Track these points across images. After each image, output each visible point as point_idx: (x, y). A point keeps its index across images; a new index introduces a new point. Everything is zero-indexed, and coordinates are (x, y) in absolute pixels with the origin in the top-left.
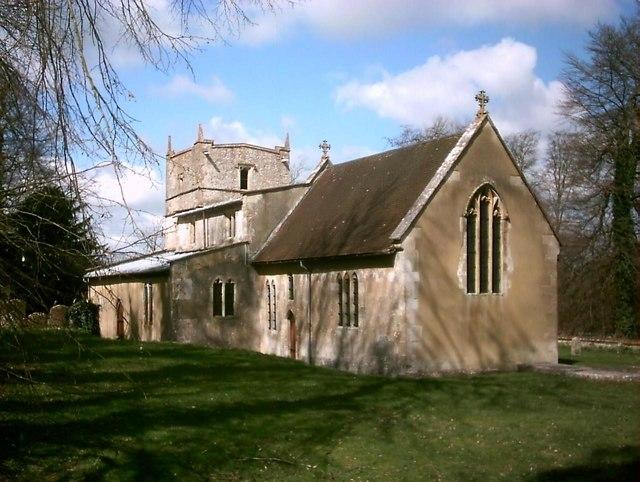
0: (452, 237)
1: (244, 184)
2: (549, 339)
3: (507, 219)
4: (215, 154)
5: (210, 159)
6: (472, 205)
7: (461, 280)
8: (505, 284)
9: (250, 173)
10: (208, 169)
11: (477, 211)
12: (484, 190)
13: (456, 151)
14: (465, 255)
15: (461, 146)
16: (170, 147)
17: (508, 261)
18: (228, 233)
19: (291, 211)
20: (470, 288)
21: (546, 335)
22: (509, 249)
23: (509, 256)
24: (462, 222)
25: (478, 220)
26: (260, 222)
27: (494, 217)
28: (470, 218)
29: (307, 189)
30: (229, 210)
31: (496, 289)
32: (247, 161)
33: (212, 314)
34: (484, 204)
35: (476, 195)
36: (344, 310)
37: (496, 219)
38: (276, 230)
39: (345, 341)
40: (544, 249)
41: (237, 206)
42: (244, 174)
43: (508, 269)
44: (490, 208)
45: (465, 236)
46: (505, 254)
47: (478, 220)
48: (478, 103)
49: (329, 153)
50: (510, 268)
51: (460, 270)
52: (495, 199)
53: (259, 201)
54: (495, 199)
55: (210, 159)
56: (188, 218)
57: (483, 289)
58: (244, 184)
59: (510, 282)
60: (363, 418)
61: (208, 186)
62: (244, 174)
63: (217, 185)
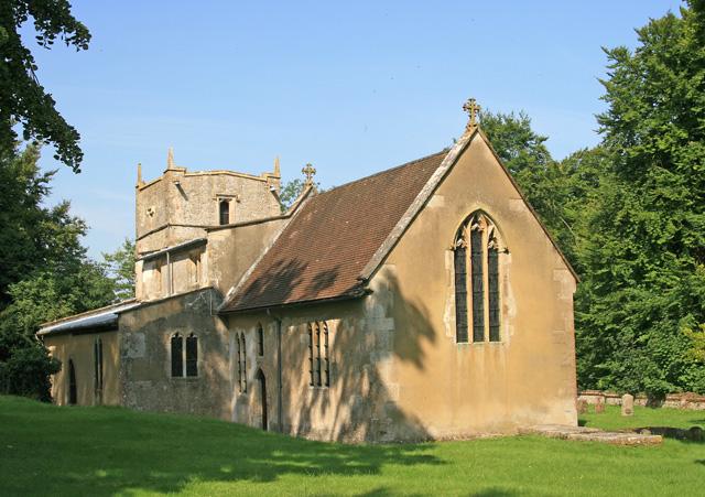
0: (438, 275)
1: (224, 218)
2: (565, 396)
3: (507, 252)
4: (187, 185)
5: (181, 191)
6: (460, 235)
7: (448, 326)
8: (506, 330)
9: (232, 204)
10: (177, 200)
11: (468, 243)
12: (475, 216)
13: (440, 171)
14: (454, 296)
15: (445, 165)
16: (139, 176)
17: (509, 301)
18: (194, 277)
19: (266, 250)
20: (462, 336)
21: (561, 392)
22: (510, 289)
23: (511, 295)
24: (449, 260)
25: (468, 253)
26: (233, 263)
27: (489, 250)
28: (458, 252)
29: (286, 223)
30: (193, 250)
31: (495, 336)
32: (227, 192)
33: (170, 374)
34: (476, 234)
35: (465, 223)
36: (315, 368)
37: (493, 252)
38: (249, 273)
39: (359, 374)
40: (557, 286)
41: (201, 245)
42: (224, 206)
43: (510, 312)
44: (485, 238)
45: (453, 273)
46: (506, 294)
47: (468, 253)
48: (467, 113)
49: (315, 179)
50: (512, 311)
51: (447, 314)
52: (491, 228)
53: (227, 239)
54: (491, 228)
55: (181, 191)
56: (155, 261)
57: (478, 337)
58: (224, 218)
59: (512, 327)
60: (393, 457)
61: (179, 222)
62: (224, 206)
63: (190, 217)
